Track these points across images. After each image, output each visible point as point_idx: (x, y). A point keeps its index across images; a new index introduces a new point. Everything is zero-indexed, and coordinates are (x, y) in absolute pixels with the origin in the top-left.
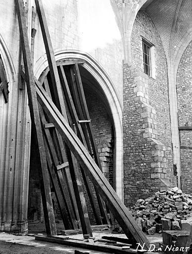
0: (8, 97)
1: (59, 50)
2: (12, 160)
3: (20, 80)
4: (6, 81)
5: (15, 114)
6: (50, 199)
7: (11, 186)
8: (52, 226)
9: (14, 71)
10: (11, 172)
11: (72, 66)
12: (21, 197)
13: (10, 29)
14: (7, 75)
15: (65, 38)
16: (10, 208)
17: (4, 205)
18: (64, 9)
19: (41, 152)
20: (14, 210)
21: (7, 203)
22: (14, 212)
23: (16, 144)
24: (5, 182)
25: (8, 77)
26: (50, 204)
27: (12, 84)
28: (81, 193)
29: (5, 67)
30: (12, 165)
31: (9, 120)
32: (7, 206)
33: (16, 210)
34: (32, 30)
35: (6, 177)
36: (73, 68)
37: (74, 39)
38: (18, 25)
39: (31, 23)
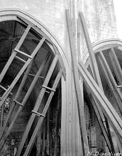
0: (66, 77)
1: (97, 41)
2: (70, 116)
3: (106, 79)
4: (64, 68)
5: (71, 87)
6: (86, 141)
7: (70, 133)
8: (27, 150)
9: (68, 61)
10: (70, 124)
11: (109, 50)
12: (77, 141)
13: (65, 37)
14: (65, 64)
15: (102, 33)
16: (70, 148)
17: (67, 146)
18: (100, 15)
19: (81, 109)
20: (73, 149)
21: (69, 144)
22: (73, 150)
23: (72, 106)
24: (67, 130)
25: (65, 65)
26: (87, 145)
27: (68, 69)
28: (114, 137)
29: (63, 60)
30: (70, 119)
31: (67, 91)
32: (69, 146)
33: (74, 150)
34: (78, 33)
35: (67, 127)
36: (110, 51)
37: (108, 32)
38: (84, 39)
39: (76, 27)
